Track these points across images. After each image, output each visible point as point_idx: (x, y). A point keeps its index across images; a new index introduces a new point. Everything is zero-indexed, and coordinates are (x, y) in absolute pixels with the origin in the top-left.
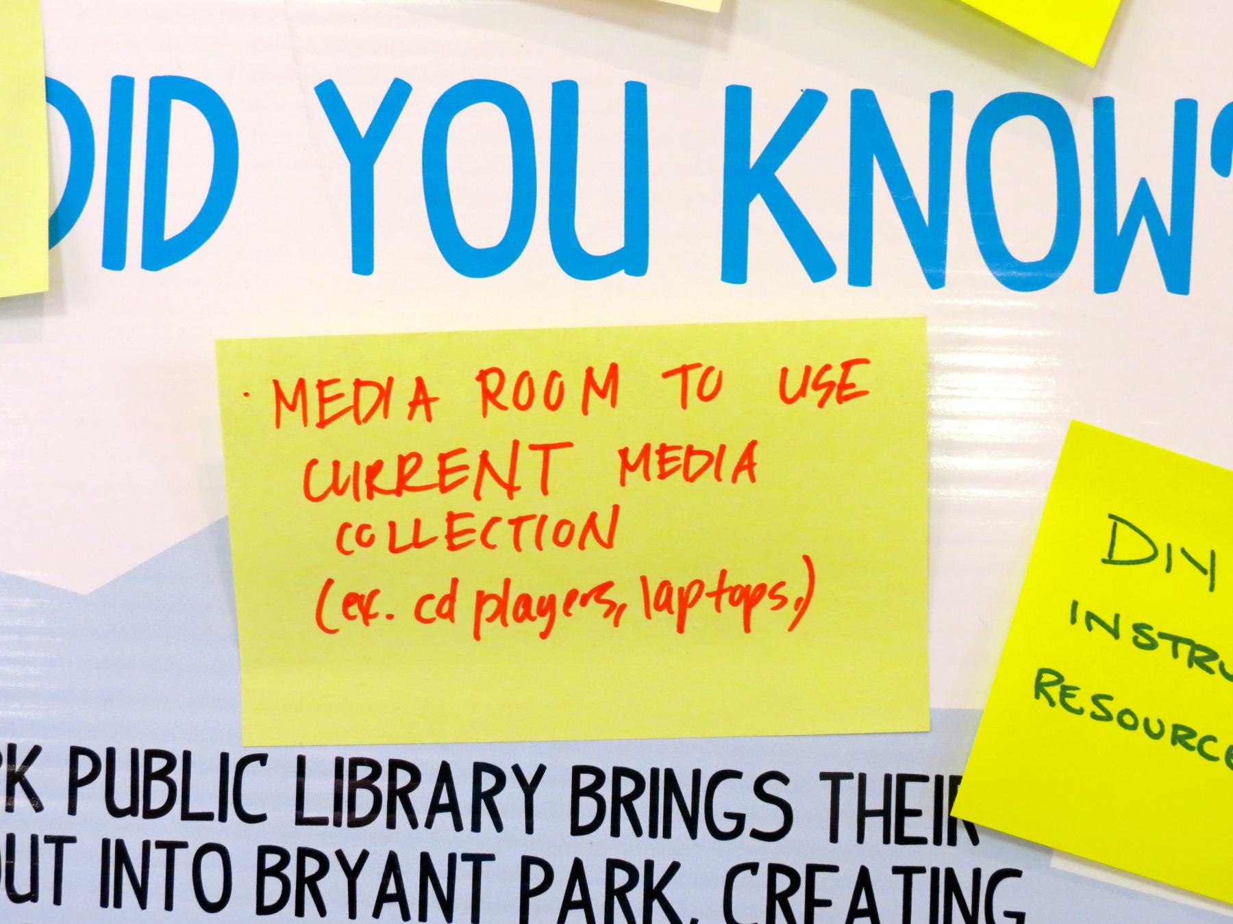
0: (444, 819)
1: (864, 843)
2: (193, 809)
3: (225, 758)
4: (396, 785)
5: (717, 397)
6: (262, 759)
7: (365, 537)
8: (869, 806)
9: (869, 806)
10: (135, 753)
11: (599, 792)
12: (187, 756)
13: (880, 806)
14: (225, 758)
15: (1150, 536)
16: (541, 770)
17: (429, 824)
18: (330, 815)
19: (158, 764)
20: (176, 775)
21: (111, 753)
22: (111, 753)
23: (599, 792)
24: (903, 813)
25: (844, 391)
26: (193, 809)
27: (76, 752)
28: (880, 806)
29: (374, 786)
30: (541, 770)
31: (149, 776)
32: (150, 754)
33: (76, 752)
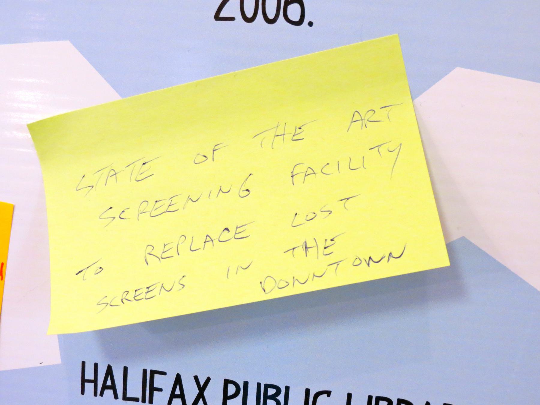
0: (109, 393)
1: (119, 398)
2: (129, 395)
3: (308, 391)
4: (227, 394)
5: (196, 202)
6: (328, 393)
7: (358, 262)
8: (87, 377)
9: (87, 377)
10: (259, 385)
11: (278, 398)
12: (287, 388)
13: (92, 378)
14: (308, 391)
15: (239, 240)
16: (208, 380)
17: (102, 394)
18: (140, 396)
19: (271, 392)
20: (281, 398)
21: (246, 384)
22: (246, 384)
23: (278, 398)
24: (153, 389)
25: (129, 209)
26: (129, 395)
27: (227, 382)
28: (92, 378)
29: (277, 399)
30: (208, 380)
31: (266, 397)
32: (267, 386)
33: (227, 382)
